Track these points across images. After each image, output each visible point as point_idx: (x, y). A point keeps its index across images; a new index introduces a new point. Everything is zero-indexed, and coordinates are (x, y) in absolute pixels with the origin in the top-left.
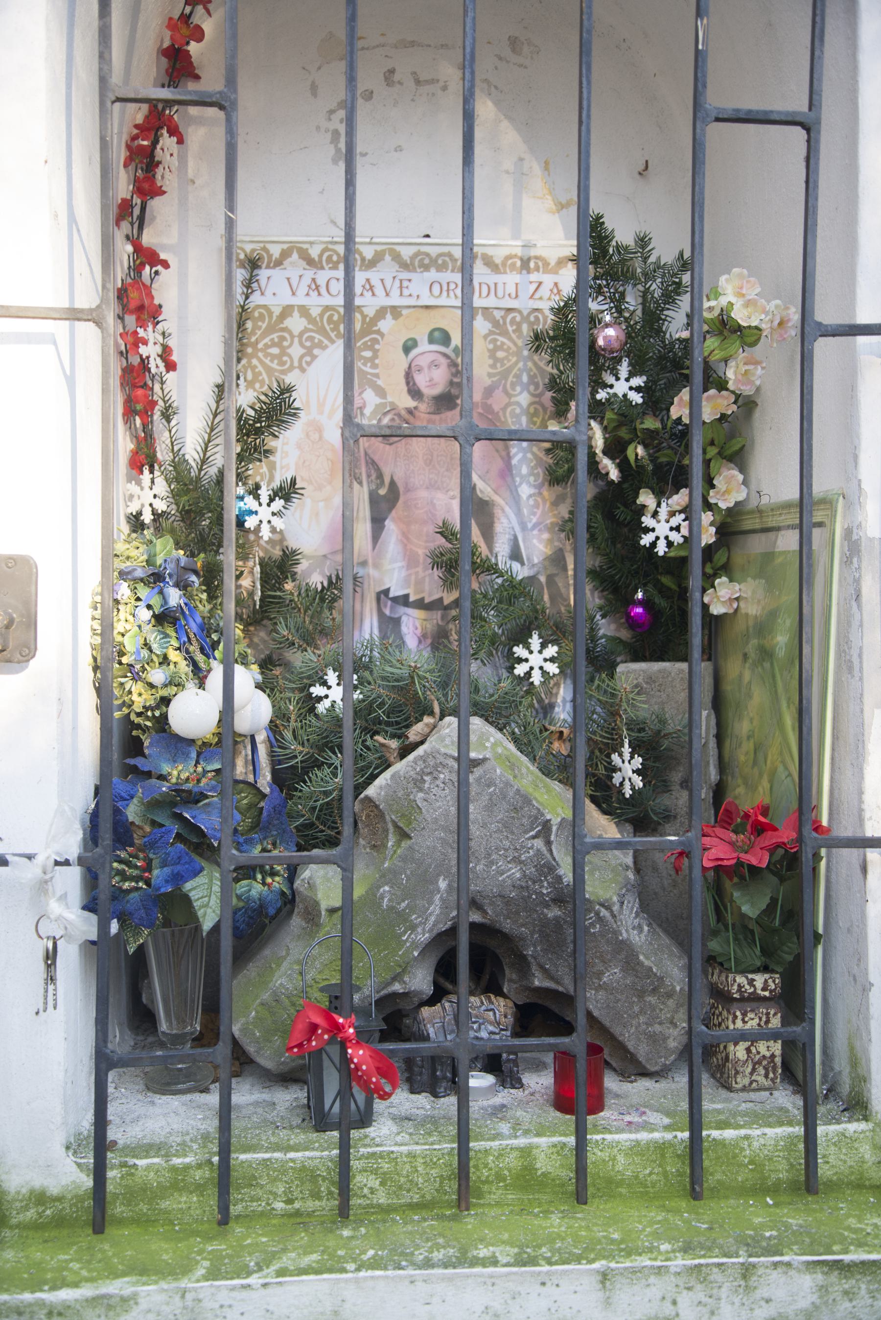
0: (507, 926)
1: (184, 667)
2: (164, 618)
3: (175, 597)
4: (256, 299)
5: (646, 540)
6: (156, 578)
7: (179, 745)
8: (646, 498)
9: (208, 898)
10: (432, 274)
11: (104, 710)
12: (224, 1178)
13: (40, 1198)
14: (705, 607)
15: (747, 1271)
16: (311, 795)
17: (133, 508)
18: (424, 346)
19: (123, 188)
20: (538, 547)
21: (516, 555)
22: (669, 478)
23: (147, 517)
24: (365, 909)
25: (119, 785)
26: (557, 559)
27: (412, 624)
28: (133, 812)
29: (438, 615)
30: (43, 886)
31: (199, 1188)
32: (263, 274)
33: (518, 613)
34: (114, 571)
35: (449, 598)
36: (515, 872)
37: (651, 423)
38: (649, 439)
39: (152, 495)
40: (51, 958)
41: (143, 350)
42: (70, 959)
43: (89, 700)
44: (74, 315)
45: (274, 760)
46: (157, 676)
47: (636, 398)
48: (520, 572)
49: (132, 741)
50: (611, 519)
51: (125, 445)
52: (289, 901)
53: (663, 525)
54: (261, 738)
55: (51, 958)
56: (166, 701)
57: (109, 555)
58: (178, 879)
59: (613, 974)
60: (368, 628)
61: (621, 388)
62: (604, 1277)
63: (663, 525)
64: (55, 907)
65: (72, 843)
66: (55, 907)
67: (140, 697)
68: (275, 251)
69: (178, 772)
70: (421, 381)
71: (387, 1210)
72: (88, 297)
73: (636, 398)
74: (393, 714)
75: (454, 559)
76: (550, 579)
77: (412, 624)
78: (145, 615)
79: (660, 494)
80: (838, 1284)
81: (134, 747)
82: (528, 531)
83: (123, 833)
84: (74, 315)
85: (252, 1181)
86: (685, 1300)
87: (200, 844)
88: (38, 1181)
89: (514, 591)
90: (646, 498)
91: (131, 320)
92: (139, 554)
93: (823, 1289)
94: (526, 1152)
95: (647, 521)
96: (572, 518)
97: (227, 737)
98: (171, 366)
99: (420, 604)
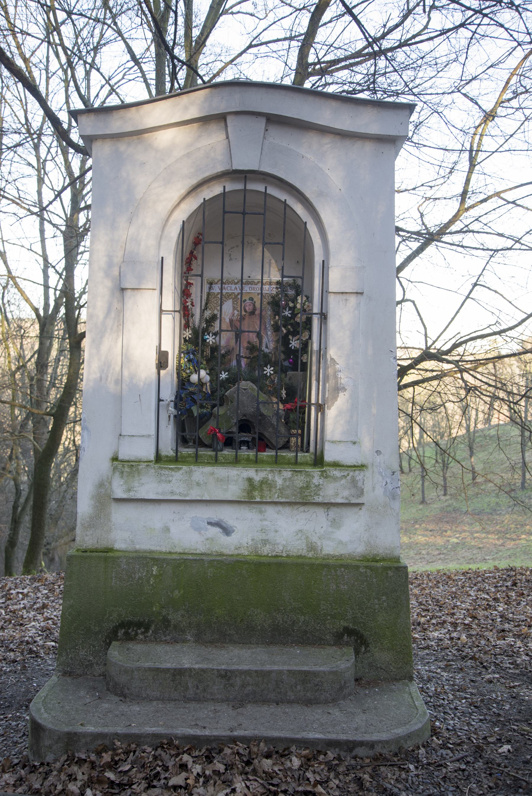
0: (251, 420)
1: (193, 370)
2: (189, 361)
3: (192, 356)
4: (212, 291)
5: (290, 346)
6: (188, 353)
7: (191, 384)
8: (290, 337)
9: (196, 411)
10: (250, 286)
11: (178, 377)
12: (133, 58)
13: (167, 456)
14: (301, 360)
15: (280, 471)
16: (217, 394)
17: (185, 336)
18: (248, 301)
19: (185, 269)
20: (272, 345)
21: (267, 347)
22: (295, 333)
23: (187, 338)
24: (226, 417)
25: (181, 391)
26: (276, 348)
27: (244, 362)
28: (183, 395)
29: (249, 360)
30: (168, 405)
31: (193, 457)
32: (213, 286)
33: (267, 360)
34: (180, 352)
35: (252, 356)
36: (252, 410)
37: (292, 321)
38: (291, 325)
39: (188, 334)
40: (169, 416)
41: (187, 304)
42: (172, 416)
43: (175, 375)
44: (175, 311)
45: (211, 389)
46: (188, 371)
47: (290, 315)
48: (266, 351)
49: (183, 383)
50: (285, 341)
51: (183, 322)
52: (211, 414)
53: (294, 344)
54: (208, 384)
55: (169, 416)
56: (189, 376)
57: (180, 348)
58: (190, 406)
59: (270, 430)
60: (234, 363)
61: (287, 313)
62: (256, 471)
63: (294, 344)
64: (170, 408)
65: (173, 398)
66: (170, 408)
67: (184, 375)
68: (216, 281)
69: (191, 389)
70: (247, 308)
71: (224, 463)
72: (178, 309)
73: (290, 315)
74: (233, 380)
75: (252, 348)
76: (275, 353)
77: (244, 362)
78: (186, 360)
79: (293, 336)
80: (295, 474)
81: (184, 384)
82: (269, 343)
83: (181, 399)
84: (175, 311)
85: (201, 457)
86: (270, 475)
87: (194, 401)
88: (167, 454)
89: (266, 355)
90: (290, 337)
91: (185, 297)
92: (185, 348)
93: (292, 475)
94: (248, 455)
95: (291, 342)
96: (278, 340)
97: (201, 383)
98: (193, 306)
99: (245, 357)
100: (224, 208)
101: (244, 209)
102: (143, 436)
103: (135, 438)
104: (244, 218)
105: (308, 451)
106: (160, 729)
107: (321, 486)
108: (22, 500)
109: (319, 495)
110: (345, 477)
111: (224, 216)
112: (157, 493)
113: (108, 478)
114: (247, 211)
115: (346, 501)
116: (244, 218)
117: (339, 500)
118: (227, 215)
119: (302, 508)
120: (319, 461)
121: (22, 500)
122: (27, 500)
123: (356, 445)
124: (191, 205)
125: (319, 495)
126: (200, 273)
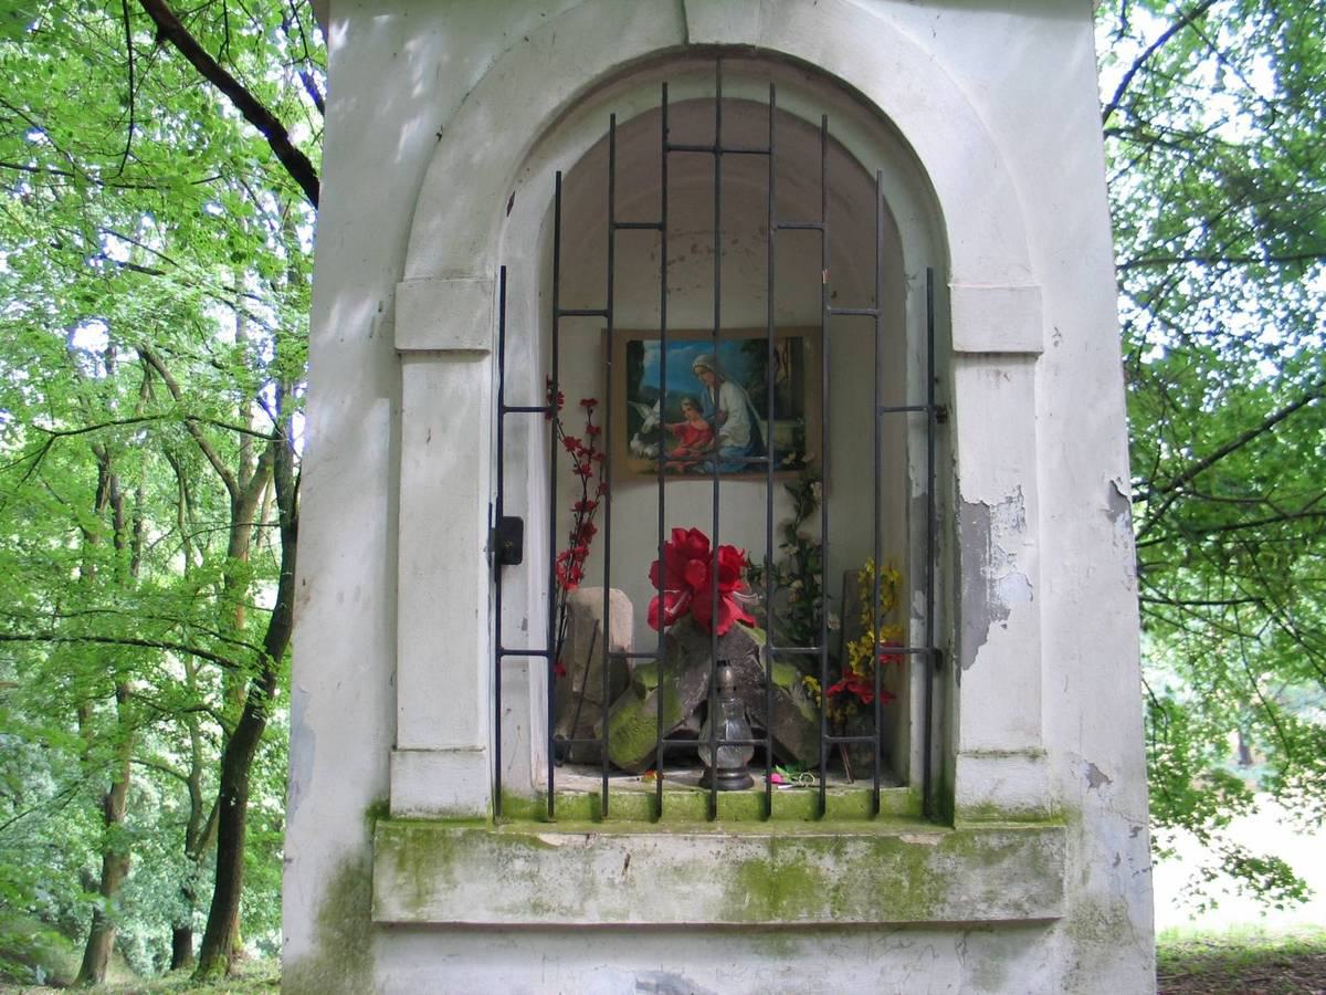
100: (612, 215)
101: (718, 140)
102: (455, 750)
103: (428, 758)
104: (718, 163)
105: (904, 783)
106: (908, 838)
107: (949, 879)
108: (202, 825)
109: (944, 901)
110: (1012, 848)
111: (664, 158)
112: (497, 909)
113: (361, 865)
114: (723, 145)
115: (1017, 916)
116: (718, 163)
117: (998, 914)
118: (672, 155)
119: (894, 939)
120: (937, 805)
121: (202, 825)
122: (209, 824)
123: (1039, 760)
124: (538, 193)
125: (944, 901)
126: (604, 306)
